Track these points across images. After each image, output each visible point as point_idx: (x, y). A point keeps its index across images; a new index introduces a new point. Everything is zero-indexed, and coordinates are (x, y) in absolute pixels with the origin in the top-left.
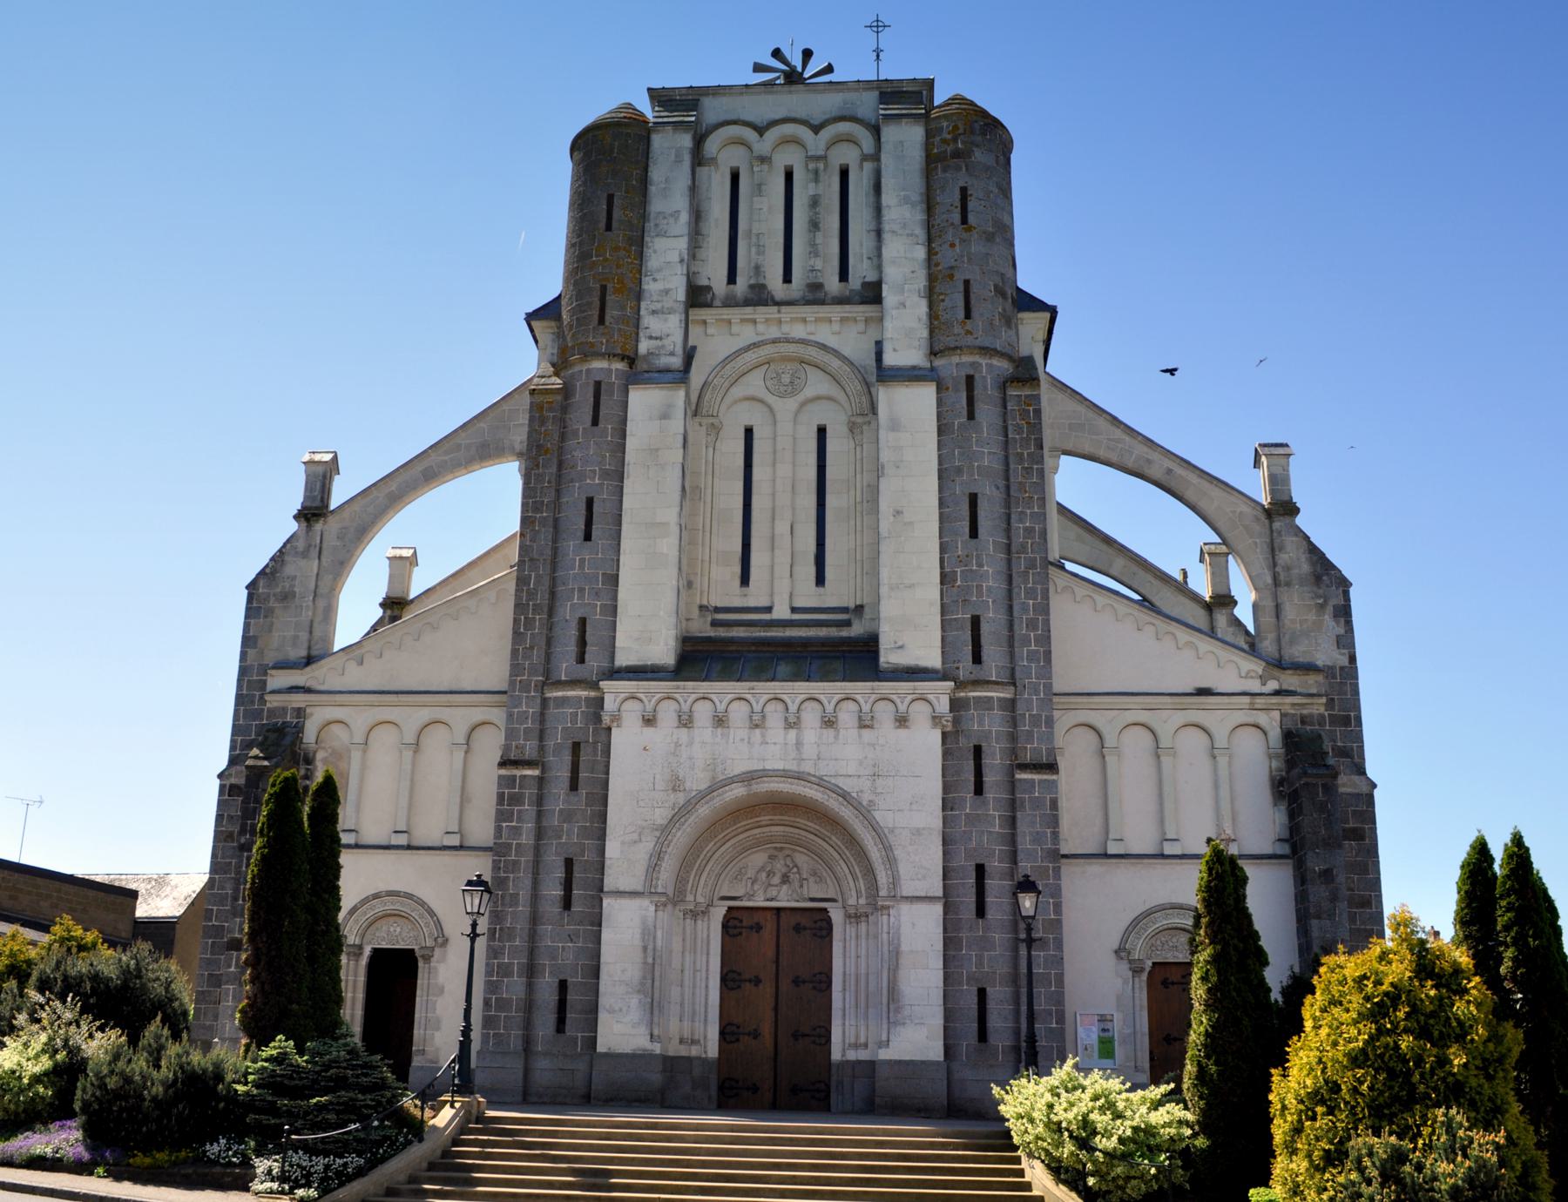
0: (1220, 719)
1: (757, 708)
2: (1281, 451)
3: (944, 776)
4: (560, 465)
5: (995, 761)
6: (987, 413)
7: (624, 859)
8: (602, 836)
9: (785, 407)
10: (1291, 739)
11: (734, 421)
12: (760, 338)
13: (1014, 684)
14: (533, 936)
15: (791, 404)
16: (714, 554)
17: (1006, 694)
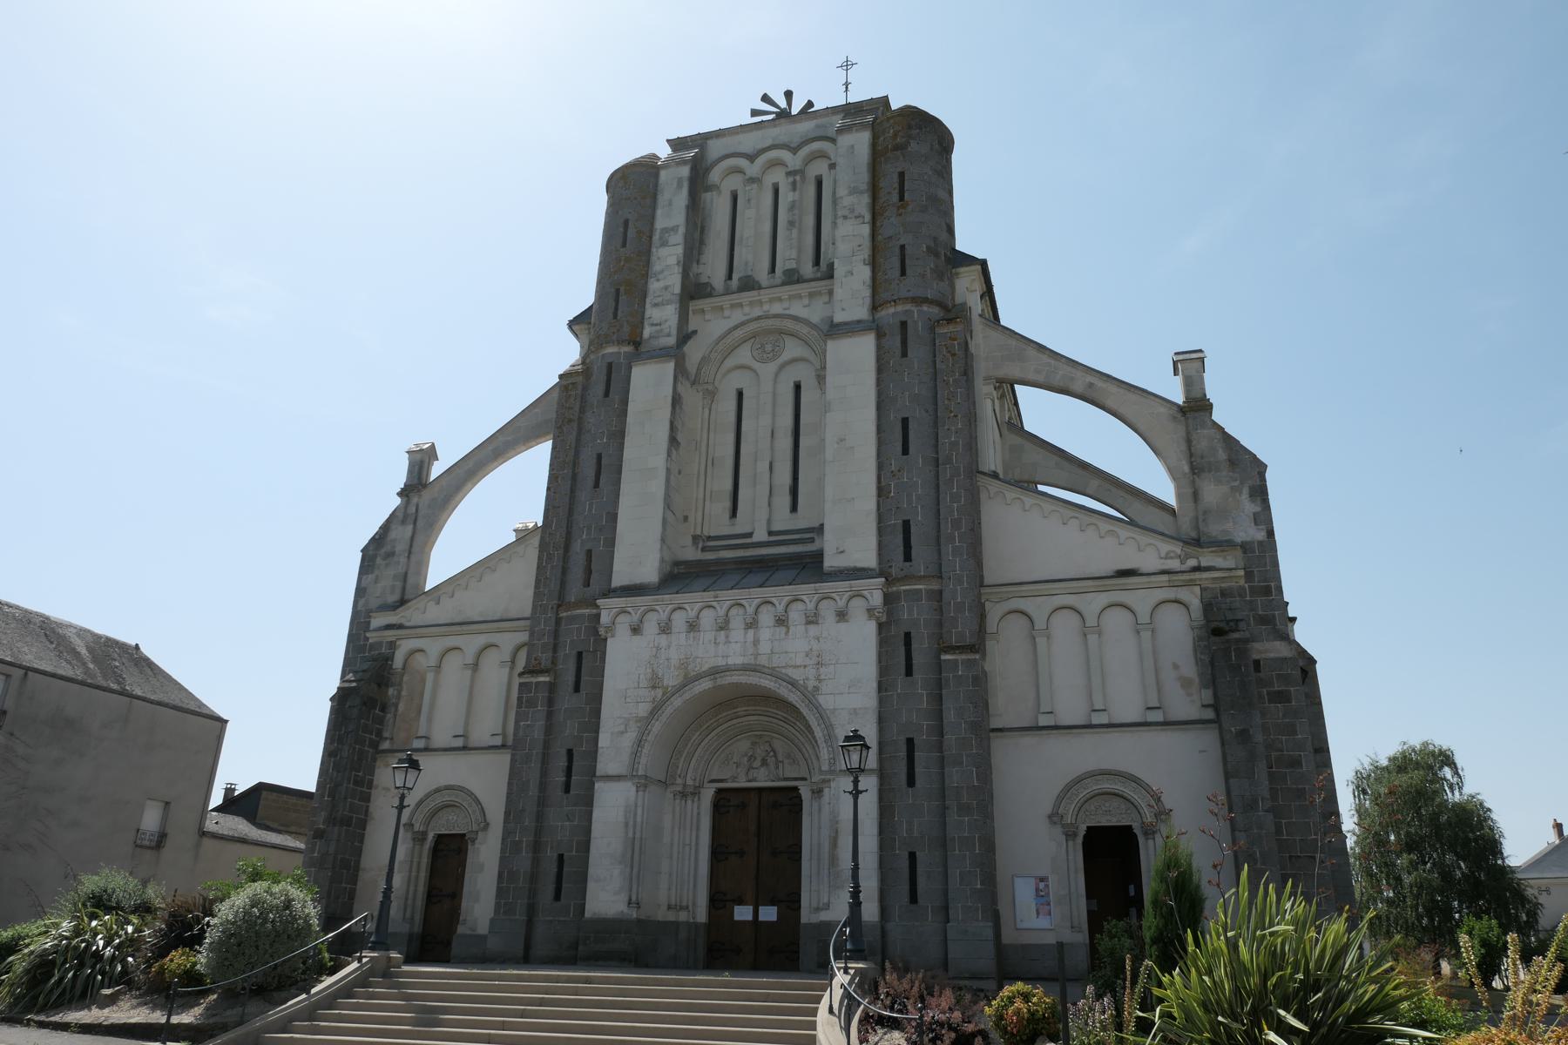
0: (1142, 599)
5: (921, 647)
6: (918, 352)
7: (614, 746)
14: (540, 817)
15: (772, 367)
17: (935, 586)
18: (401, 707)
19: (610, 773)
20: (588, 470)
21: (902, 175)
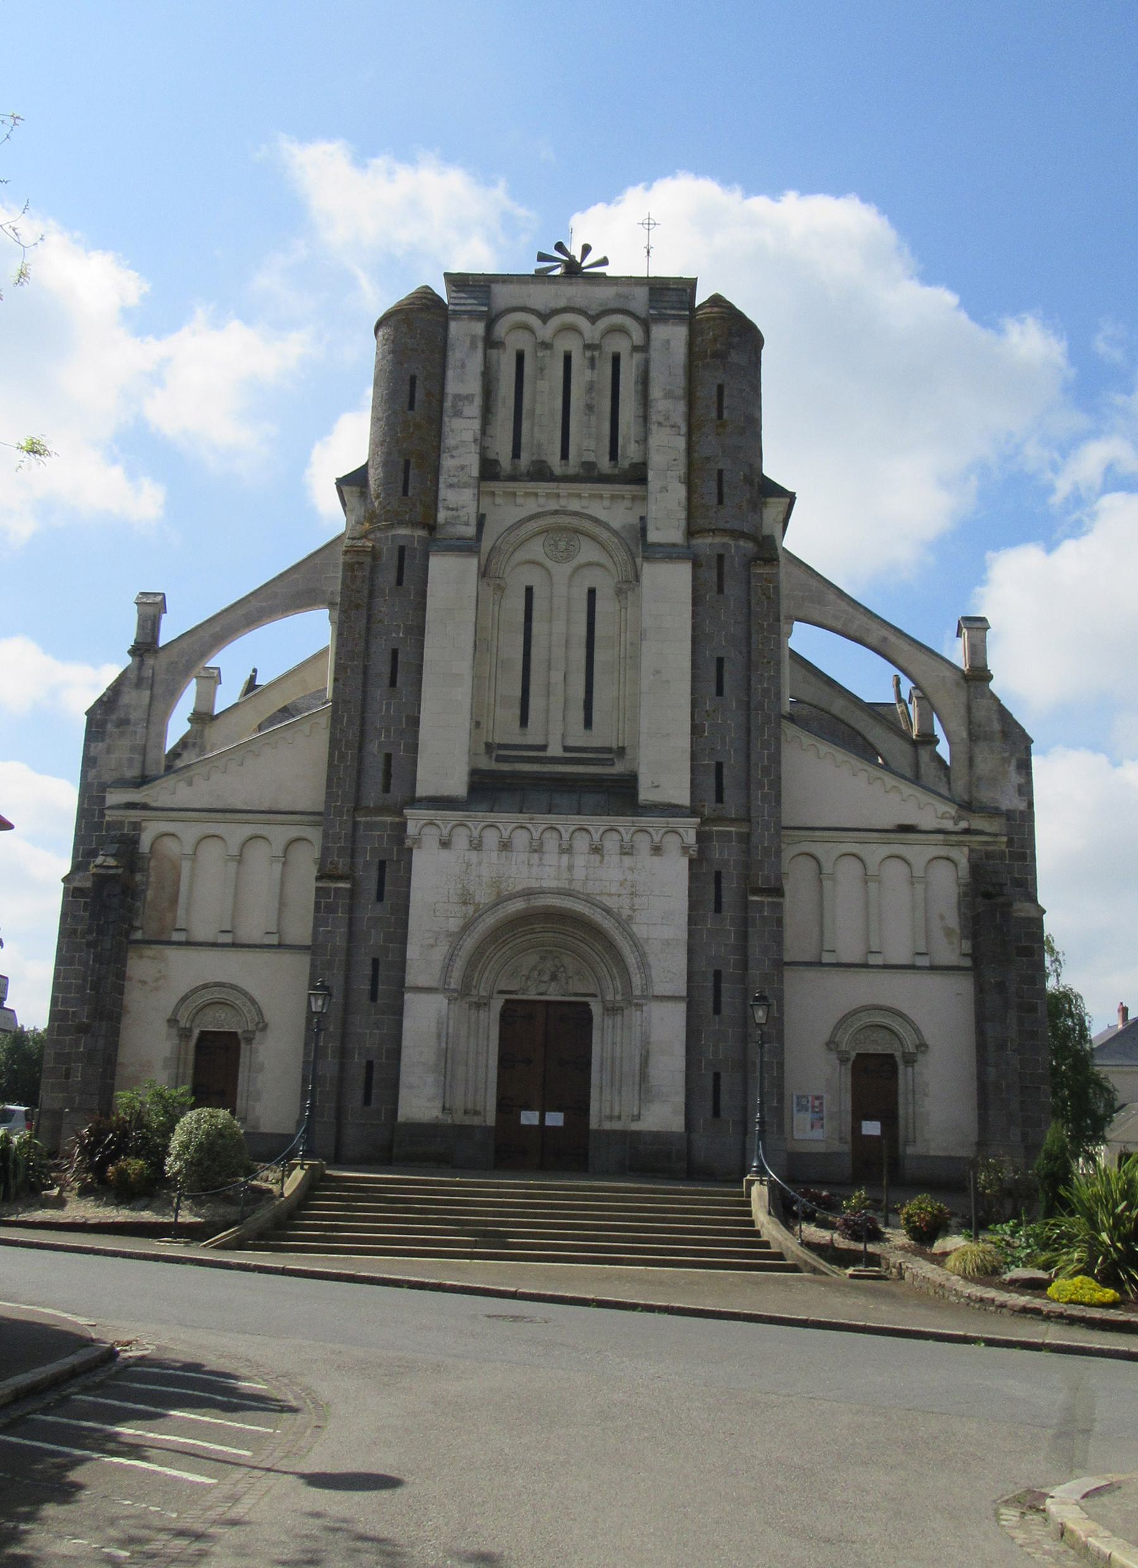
0: (919, 853)
1: (536, 835)
2: (978, 624)
3: (690, 896)
4: (369, 618)
6: (733, 588)
7: (425, 956)
8: (403, 940)
9: (561, 571)
10: (976, 869)
11: (517, 580)
12: (540, 510)
13: (749, 821)
14: (345, 1023)
15: (567, 568)
16: (498, 698)
18: (150, 894)
19: (420, 985)
20: (382, 667)
21: (720, 388)
